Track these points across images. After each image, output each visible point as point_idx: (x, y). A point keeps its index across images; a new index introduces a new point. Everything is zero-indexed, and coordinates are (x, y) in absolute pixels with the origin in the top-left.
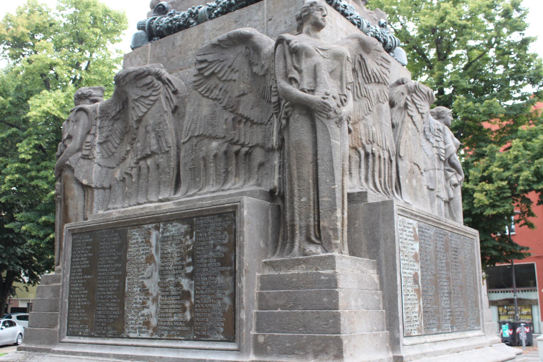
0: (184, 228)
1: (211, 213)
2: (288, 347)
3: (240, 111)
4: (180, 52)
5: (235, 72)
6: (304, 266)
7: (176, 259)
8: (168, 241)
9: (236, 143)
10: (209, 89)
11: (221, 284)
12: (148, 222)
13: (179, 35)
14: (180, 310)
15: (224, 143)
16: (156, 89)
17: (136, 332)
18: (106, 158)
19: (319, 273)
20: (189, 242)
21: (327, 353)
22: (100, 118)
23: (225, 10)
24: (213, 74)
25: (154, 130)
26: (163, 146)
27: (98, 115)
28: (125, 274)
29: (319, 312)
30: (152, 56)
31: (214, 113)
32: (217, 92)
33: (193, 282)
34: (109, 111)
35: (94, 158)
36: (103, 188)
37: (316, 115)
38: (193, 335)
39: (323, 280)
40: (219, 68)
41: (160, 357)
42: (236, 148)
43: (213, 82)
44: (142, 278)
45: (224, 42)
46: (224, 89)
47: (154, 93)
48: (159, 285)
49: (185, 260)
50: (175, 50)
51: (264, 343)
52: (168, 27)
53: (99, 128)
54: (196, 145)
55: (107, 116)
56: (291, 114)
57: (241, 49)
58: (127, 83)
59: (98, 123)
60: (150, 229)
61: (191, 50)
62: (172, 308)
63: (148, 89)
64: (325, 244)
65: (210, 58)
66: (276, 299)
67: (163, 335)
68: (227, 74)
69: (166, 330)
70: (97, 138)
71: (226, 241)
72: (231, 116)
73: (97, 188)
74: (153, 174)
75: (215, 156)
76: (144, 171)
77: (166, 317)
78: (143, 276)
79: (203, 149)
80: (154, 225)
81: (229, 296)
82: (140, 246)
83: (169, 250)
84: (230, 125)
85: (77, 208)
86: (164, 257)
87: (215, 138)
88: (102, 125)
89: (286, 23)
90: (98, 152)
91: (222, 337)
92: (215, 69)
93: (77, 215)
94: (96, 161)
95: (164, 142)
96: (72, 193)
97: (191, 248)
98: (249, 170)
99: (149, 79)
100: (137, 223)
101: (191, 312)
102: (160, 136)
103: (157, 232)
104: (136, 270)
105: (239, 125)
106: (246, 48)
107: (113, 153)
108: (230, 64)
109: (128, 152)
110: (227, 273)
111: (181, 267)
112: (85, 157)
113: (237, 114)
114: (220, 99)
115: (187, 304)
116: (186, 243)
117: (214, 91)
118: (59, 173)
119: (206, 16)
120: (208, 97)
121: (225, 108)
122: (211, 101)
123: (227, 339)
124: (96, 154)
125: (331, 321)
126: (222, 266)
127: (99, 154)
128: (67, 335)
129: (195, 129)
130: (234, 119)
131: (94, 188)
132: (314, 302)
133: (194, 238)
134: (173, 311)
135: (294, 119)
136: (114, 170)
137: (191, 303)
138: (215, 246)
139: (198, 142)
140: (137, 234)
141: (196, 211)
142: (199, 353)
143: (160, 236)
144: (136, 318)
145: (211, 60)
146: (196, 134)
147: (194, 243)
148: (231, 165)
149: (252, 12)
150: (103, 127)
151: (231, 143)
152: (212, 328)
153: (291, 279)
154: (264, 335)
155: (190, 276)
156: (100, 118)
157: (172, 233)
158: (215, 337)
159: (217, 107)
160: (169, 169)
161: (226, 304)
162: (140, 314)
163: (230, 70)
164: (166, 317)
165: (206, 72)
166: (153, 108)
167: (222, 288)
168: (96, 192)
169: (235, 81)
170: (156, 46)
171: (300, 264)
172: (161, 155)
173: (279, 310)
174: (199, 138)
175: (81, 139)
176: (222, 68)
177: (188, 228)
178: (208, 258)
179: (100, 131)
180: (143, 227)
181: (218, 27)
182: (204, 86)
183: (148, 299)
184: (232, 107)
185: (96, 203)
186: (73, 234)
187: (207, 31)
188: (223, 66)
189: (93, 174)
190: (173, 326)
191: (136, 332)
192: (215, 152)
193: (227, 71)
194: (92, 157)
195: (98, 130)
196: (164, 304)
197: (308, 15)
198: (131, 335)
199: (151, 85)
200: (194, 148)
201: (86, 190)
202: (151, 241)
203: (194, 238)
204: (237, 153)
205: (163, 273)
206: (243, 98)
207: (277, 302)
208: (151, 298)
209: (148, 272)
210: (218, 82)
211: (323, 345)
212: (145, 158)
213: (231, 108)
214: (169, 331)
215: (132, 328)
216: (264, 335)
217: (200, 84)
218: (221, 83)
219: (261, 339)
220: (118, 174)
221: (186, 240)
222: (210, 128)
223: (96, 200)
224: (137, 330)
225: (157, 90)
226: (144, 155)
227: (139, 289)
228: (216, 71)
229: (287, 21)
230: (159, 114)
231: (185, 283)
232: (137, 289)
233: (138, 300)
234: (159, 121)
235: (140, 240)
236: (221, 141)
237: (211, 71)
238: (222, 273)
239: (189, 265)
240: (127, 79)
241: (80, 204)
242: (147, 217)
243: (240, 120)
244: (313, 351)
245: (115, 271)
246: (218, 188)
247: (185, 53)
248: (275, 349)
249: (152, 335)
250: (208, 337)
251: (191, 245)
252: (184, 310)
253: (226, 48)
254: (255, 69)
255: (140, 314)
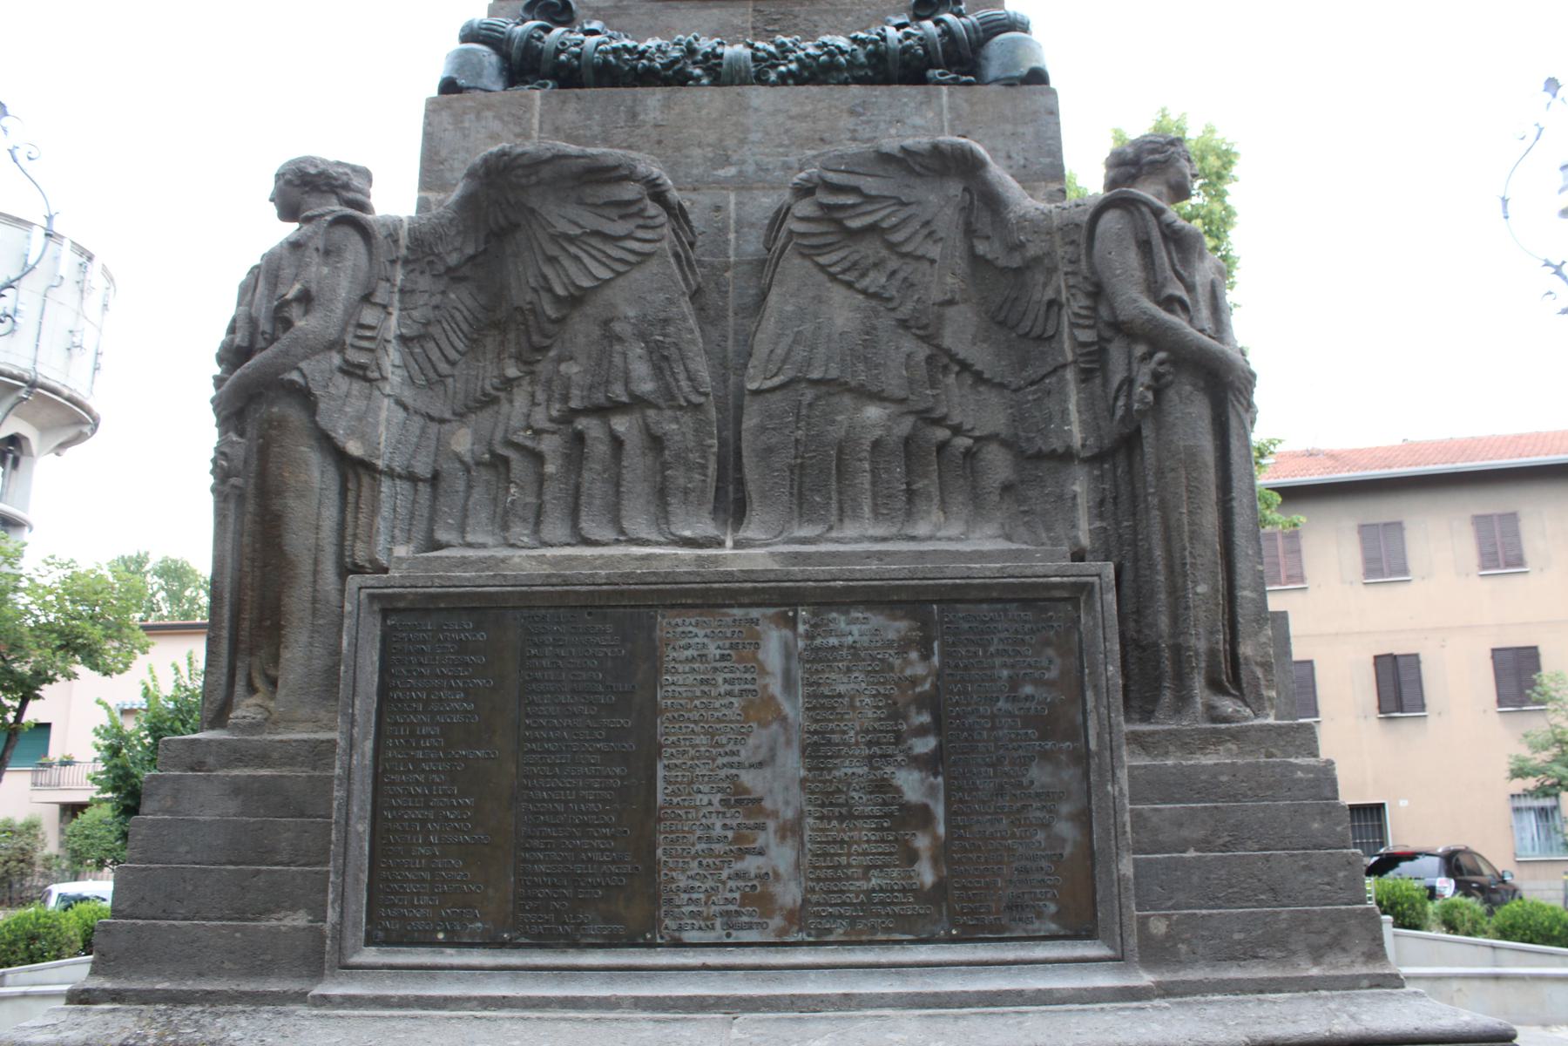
0: (897, 628)
1: (995, 595)
2: (1239, 942)
3: (947, 342)
4: (659, 142)
5: (935, 242)
6: (1234, 747)
7: (868, 714)
8: (835, 660)
9: (939, 422)
10: (855, 264)
11: (1042, 786)
12: (746, 600)
13: (653, 99)
14: (895, 859)
15: (903, 414)
16: (650, 223)
17: (713, 928)
18: (420, 387)
19: (1291, 764)
20: (920, 670)
21: (1344, 950)
22: (406, 262)
23: (806, 74)
24: (873, 229)
25: (642, 336)
26: (679, 388)
27: (403, 252)
28: (655, 751)
29: (1310, 856)
30: (547, 127)
31: (870, 330)
32: (883, 280)
33: (940, 779)
34: (440, 249)
35: (384, 378)
36: (412, 478)
37: (1231, 396)
38: (947, 926)
39: (1301, 780)
40: (894, 220)
41: (846, 995)
42: (942, 434)
43: (869, 249)
44: (731, 765)
45: (919, 159)
46: (901, 275)
47: (640, 234)
48: (803, 788)
49: (905, 718)
50: (638, 131)
51: (1168, 936)
52: (606, 62)
53: (402, 291)
54: (810, 405)
55: (431, 263)
56: (1172, 383)
57: (955, 188)
58: (539, 183)
59: (399, 276)
60: (756, 622)
61: (700, 145)
62: (865, 854)
63: (622, 217)
64: (1251, 699)
65: (870, 185)
66: (1181, 825)
67: (830, 931)
68: (919, 238)
69: (841, 916)
70: (393, 320)
71: (1053, 674)
72: (923, 351)
73: (391, 474)
74: (636, 462)
75: (876, 444)
76: (599, 448)
77: (840, 879)
78: (735, 759)
79: (839, 418)
80: (771, 611)
81: (1073, 818)
82: (715, 669)
83: (842, 688)
84: (922, 372)
85: (318, 527)
86: (821, 705)
87: (878, 397)
88: (409, 286)
89: (1009, 157)
90: (397, 362)
91: (1053, 927)
92: (883, 219)
93: (318, 548)
94: (388, 389)
95: (682, 377)
96: (303, 477)
97: (927, 686)
98: (976, 500)
99: (630, 191)
100: (707, 596)
101: (935, 861)
102: (666, 358)
103: (787, 633)
104: (701, 740)
105: (945, 375)
106: (965, 189)
107: (442, 377)
108: (927, 217)
109: (508, 384)
110: (1063, 757)
111: (891, 737)
112: (352, 371)
113: (938, 347)
114: (890, 299)
115: (922, 842)
116: (908, 672)
117: (872, 274)
118: (239, 405)
119: (748, 71)
120: (849, 285)
121: (904, 324)
122: (861, 297)
123: (1069, 933)
124: (390, 369)
125: (1341, 874)
126: (1043, 737)
127: (398, 371)
128: (367, 944)
129: (809, 362)
130: (930, 360)
131: (381, 472)
132: (1289, 831)
133: (936, 660)
134: (866, 861)
135: (1179, 394)
136: (446, 427)
137: (935, 837)
138: (1014, 683)
139: (818, 398)
140: (701, 633)
141: (945, 585)
142: (983, 975)
143: (801, 644)
144: (709, 883)
145: (873, 193)
146: (816, 375)
147: (939, 675)
148: (925, 475)
149: (905, 104)
150: (412, 291)
151: (925, 420)
152: (1015, 907)
153: (1215, 776)
154: (1167, 917)
155: (930, 764)
156: (406, 262)
157: (850, 639)
158: (1030, 927)
159: (877, 317)
160: (704, 457)
161: (1064, 840)
162: (725, 874)
163: (925, 231)
164: (840, 879)
165: (851, 217)
166: (636, 274)
167: (1049, 797)
168: (386, 486)
169: (933, 262)
170: (564, 102)
171: (1220, 742)
172: (669, 413)
173: (1191, 854)
174: (824, 389)
175: (346, 311)
176: (904, 221)
177: (912, 629)
178: (993, 717)
179: (401, 301)
180: (728, 615)
181: (795, 110)
182: (841, 254)
183: (762, 827)
184: (925, 327)
185: (384, 519)
186: (385, 613)
187: (756, 110)
188: (910, 217)
189: (382, 429)
190: (868, 903)
191: (713, 928)
192: (878, 433)
193: (916, 232)
194: (376, 375)
195: (396, 297)
196: (828, 843)
197: (1166, 162)
198: (688, 936)
199: (634, 209)
200: (804, 412)
201: (351, 476)
202: (761, 656)
203: (936, 660)
204: (942, 447)
205: (818, 752)
206: (951, 312)
207: (1185, 833)
208: (771, 825)
209: (758, 747)
210: (884, 253)
211: (1332, 931)
212: (603, 411)
213: (923, 328)
214: (853, 920)
215: (693, 915)
216: (1167, 917)
217: (825, 245)
218: (894, 257)
219: (1159, 927)
220: (463, 441)
221: (907, 662)
222: (861, 367)
223: (385, 510)
224: (718, 922)
225: (653, 228)
226: (599, 398)
227: (719, 796)
228: (885, 225)
229: (1014, 155)
230: (662, 296)
231: (911, 784)
232: (709, 799)
233: (718, 830)
234: (662, 315)
235: (713, 650)
236: (892, 408)
237: (867, 220)
238: (1046, 756)
239: (922, 731)
240: (546, 172)
241: (330, 515)
242: (750, 585)
243: (942, 361)
244: (1309, 946)
245: (607, 740)
246: (894, 530)
247: (679, 149)
248: (1200, 950)
249: (783, 931)
250: (1003, 929)
251: (924, 678)
252: (912, 857)
253: (919, 175)
254: (981, 248)
255: (725, 874)
